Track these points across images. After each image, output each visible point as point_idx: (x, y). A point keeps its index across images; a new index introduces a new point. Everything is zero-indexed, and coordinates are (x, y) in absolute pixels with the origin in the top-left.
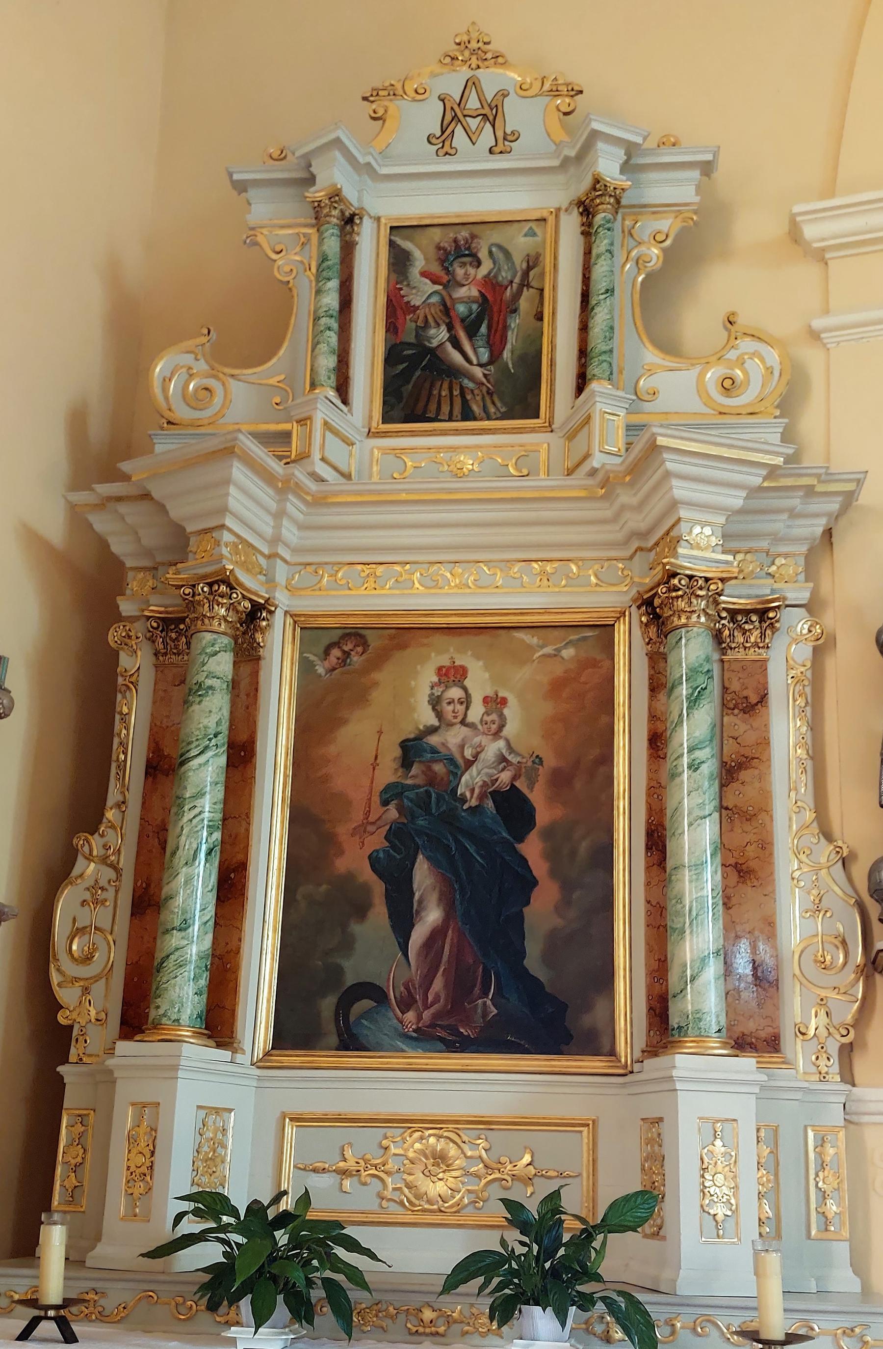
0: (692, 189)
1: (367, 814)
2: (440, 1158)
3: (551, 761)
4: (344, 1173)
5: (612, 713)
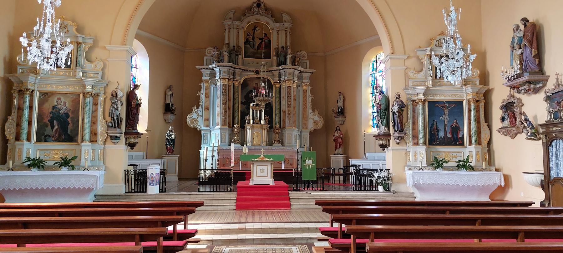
0: (92, 41)
1: (48, 115)
2: (57, 153)
3: (72, 109)
4: (45, 155)
5: (79, 104)
